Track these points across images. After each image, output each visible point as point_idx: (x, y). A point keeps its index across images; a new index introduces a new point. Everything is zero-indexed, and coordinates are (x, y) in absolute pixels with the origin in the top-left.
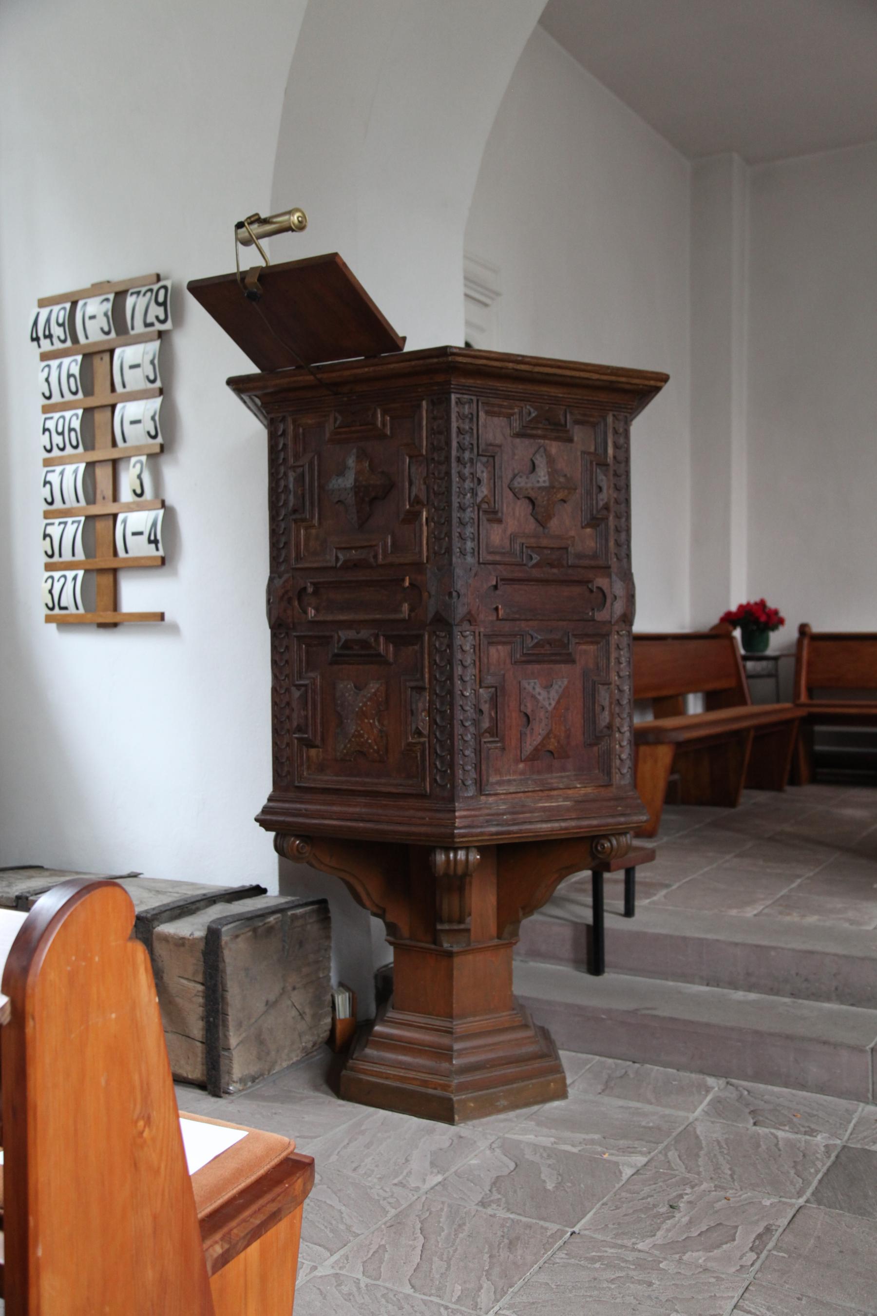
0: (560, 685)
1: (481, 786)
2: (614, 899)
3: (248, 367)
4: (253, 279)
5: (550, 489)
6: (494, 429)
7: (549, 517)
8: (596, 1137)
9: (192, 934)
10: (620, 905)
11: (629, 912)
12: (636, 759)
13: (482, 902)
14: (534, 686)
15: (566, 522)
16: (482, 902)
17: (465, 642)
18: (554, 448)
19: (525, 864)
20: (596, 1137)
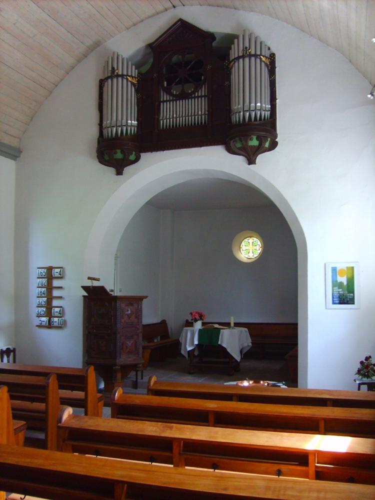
0: (131, 342)
1: (120, 357)
2: (139, 377)
3: (86, 294)
4: (274, 103)
5: (131, 313)
6: (123, 305)
7: (130, 317)
8: (154, 45)
9: (112, 291)
10: (140, 378)
11: (142, 379)
12: (143, 352)
13: (119, 375)
14: (128, 342)
15: (133, 318)
16: (119, 375)
17: (118, 336)
18: (131, 307)
19: (126, 369)
20: (154, 45)
